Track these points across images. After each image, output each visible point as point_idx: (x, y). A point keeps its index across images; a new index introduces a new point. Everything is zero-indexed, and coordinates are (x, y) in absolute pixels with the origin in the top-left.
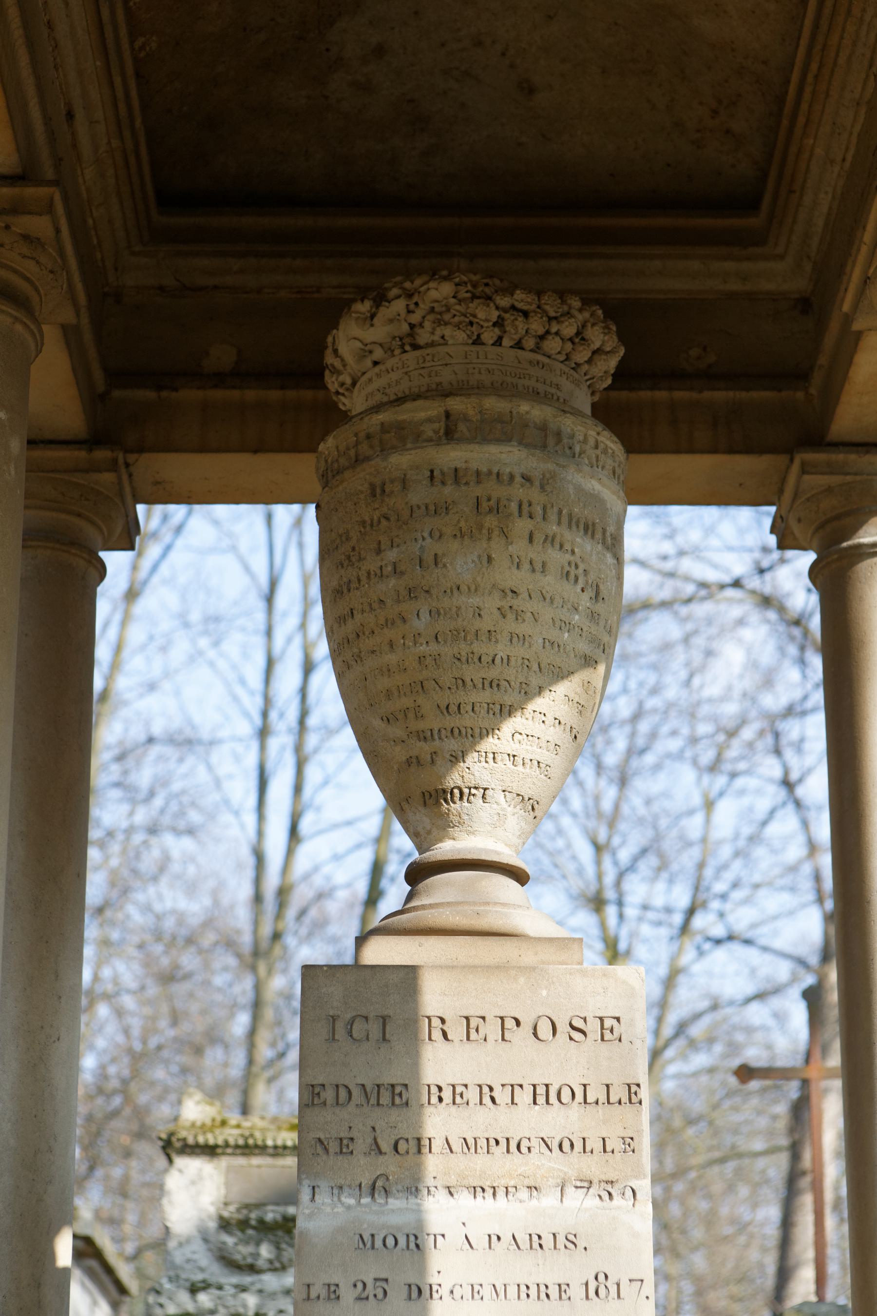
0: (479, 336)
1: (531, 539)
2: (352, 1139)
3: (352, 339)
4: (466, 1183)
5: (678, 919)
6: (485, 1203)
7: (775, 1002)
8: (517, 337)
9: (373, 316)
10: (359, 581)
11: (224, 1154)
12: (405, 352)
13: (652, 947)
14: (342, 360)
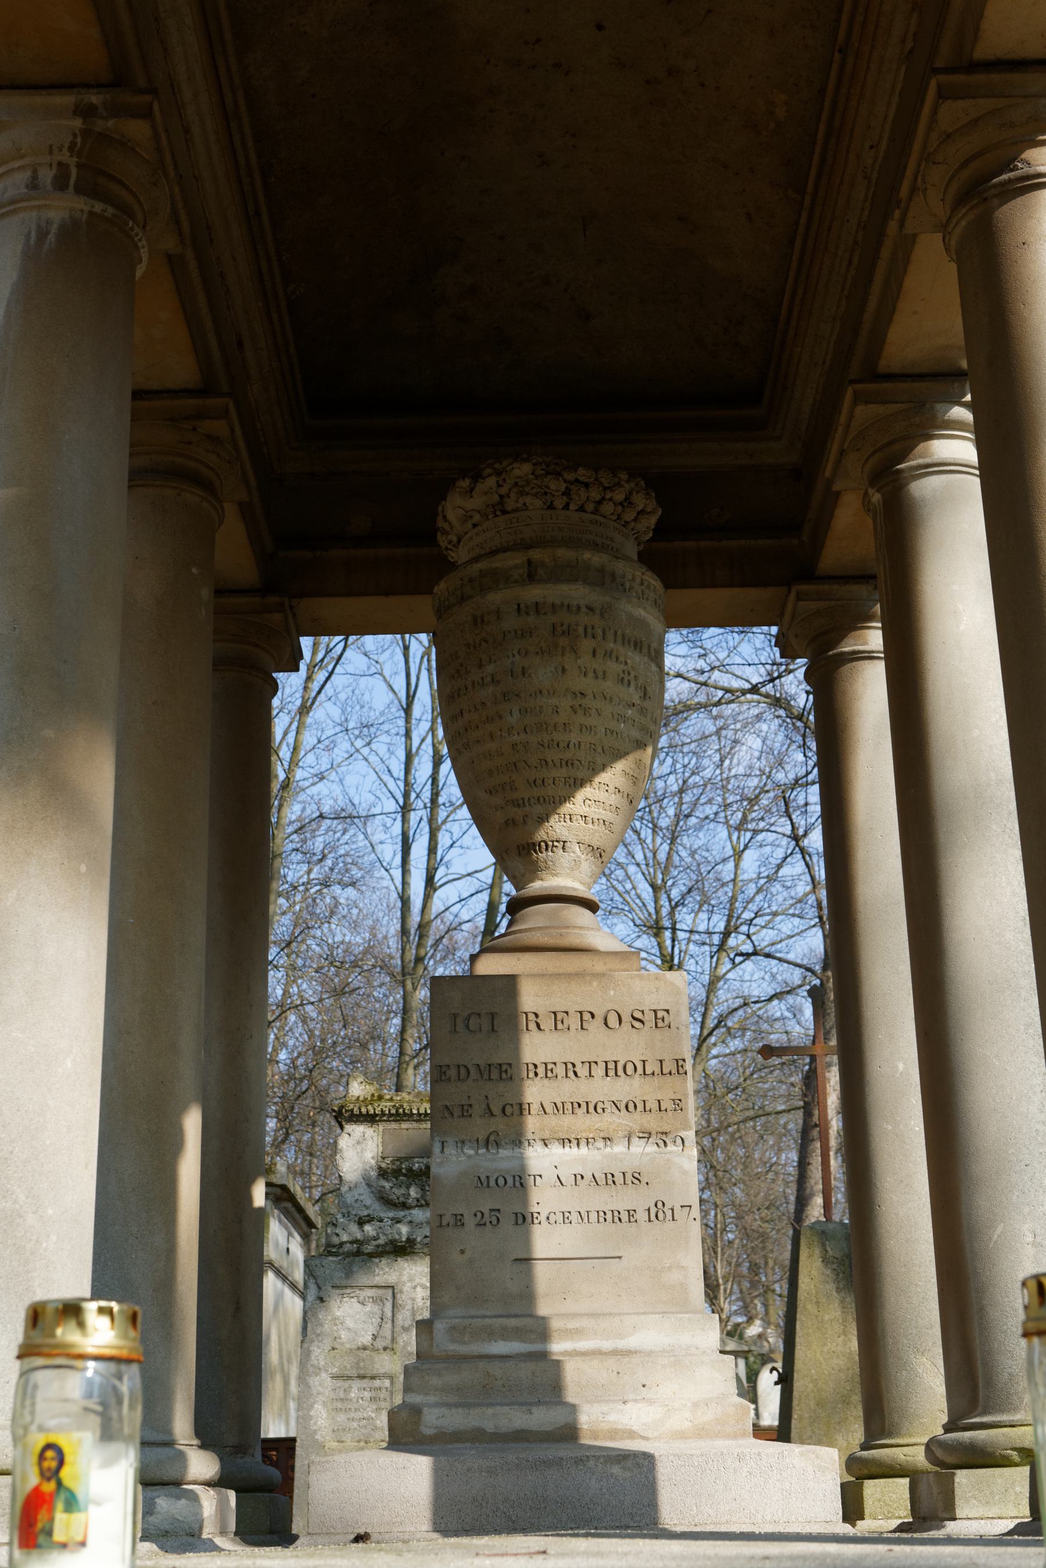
0: (552, 502)
1: (594, 655)
2: (471, 1106)
3: (456, 508)
4: (556, 1136)
5: (716, 939)
6: (572, 1152)
7: (790, 999)
8: (580, 503)
9: (472, 490)
10: (466, 689)
11: (380, 1121)
12: (497, 516)
13: (698, 960)
14: (450, 523)
